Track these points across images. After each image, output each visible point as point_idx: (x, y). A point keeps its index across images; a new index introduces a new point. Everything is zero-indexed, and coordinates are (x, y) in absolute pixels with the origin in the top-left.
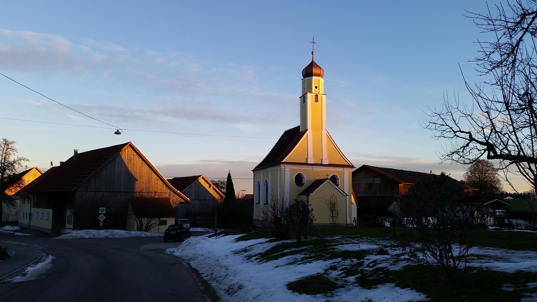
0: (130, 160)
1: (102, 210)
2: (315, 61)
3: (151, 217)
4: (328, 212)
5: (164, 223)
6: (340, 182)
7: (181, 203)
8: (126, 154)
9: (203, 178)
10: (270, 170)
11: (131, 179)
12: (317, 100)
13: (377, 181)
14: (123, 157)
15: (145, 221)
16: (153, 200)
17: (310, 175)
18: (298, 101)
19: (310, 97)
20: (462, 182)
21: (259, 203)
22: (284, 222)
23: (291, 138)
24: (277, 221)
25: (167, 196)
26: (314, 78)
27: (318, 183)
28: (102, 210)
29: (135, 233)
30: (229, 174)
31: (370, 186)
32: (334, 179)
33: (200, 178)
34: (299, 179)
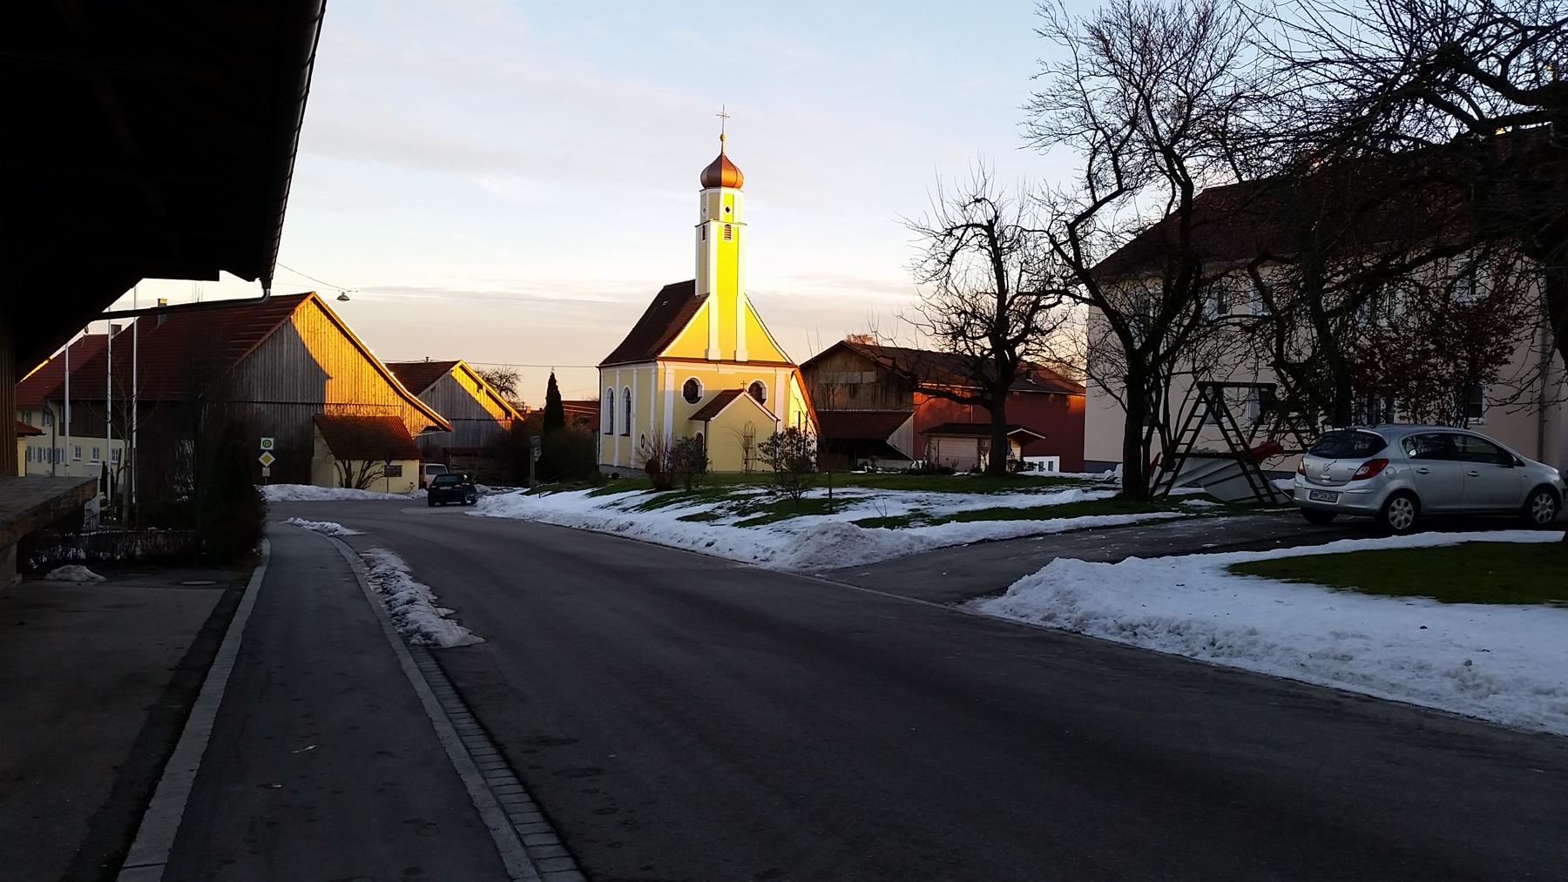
0: (314, 333)
1: (268, 443)
2: (726, 154)
3: (371, 460)
4: (740, 452)
5: (397, 472)
6: (767, 395)
7: (429, 428)
8: (305, 320)
9: (314, 300)
10: (634, 370)
11: (318, 376)
12: (728, 236)
13: (870, 377)
14: (298, 326)
15: (357, 466)
16: (372, 421)
17: (712, 381)
18: (692, 236)
19: (715, 229)
20: (597, 467)
21: (627, 435)
22: (665, 462)
23: (675, 305)
24: (652, 466)
25: (397, 413)
26: (724, 190)
27: (727, 396)
28: (268, 443)
29: (339, 492)
30: (552, 381)
31: (854, 389)
32: (757, 391)
33: (307, 308)
34: (691, 390)
